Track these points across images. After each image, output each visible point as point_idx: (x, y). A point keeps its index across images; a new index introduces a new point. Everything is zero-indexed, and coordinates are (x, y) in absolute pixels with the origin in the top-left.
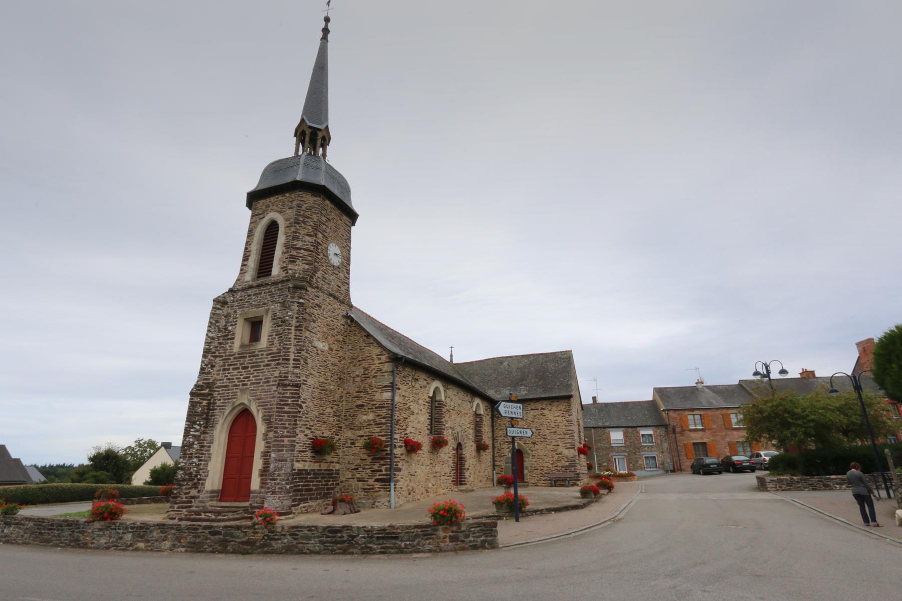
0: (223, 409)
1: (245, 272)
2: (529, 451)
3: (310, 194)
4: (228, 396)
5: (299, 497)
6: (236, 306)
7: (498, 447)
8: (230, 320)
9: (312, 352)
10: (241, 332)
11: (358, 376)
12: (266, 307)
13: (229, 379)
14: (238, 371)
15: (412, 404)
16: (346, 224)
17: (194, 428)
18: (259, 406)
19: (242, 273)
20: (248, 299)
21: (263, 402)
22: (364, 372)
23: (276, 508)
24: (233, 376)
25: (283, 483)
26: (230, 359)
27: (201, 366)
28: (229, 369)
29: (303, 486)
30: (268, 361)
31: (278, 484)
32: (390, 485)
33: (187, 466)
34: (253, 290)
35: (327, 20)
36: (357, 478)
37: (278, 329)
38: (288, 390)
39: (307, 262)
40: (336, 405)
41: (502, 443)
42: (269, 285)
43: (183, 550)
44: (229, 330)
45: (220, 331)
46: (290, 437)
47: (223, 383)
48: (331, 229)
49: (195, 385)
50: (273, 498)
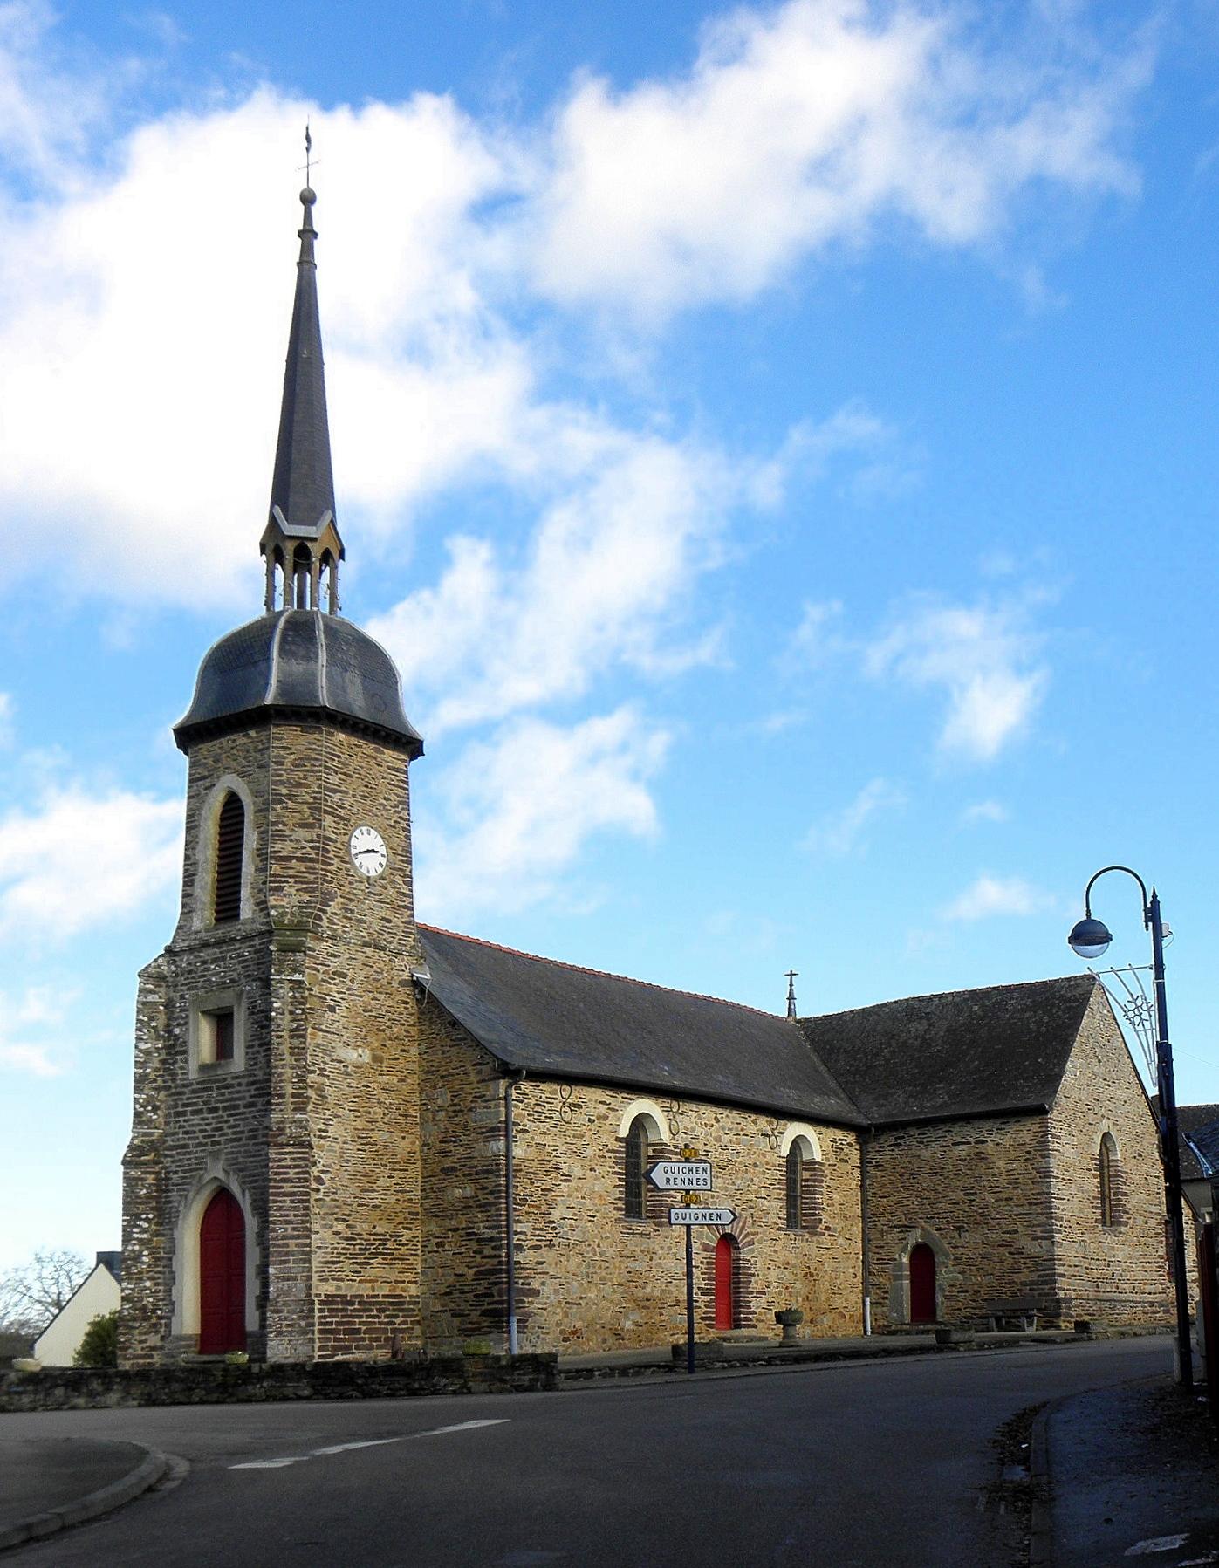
0: (184, 1190)
1: (190, 912)
2: (947, 1246)
3: (299, 729)
4: (189, 1165)
5: (332, 1343)
6: (182, 985)
7: (877, 1239)
8: (176, 1015)
9: (333, 1072)
10: (203, 1038)
11: (441, 1108)
12: (237, 989)
13: (186, 1133)
14: (202, 1116)
15: (564, 1158)
16: (393, 769)
17: (138, 1226)
18: (244, 1182)
19: (186, 913)
20: (204, 971)
21: (250, 1176)
22: (452, 1100)
23: (286, 1358)
24: (193, 1125)
25: (295, 1316)
26: (183, 1093)
27: (135, 1109)
28: (184, 1113)
29: (337, 1323)
30: (251, 1097)
31: (286, 1319)
32: (508, 1322)
33: (136, 1295)
34: (210, 951)
35: (308, 199)
36: (450, 1310)
37: (262, 1034)
38: (287, 1153)
39: (304, 886)
40: (401, 1170)
41: (885, 1228)
42: (236, 940)
43: (135, 1403)
44: (176, 1035)
45: (158, 1037)
46: (298, 1237)
47: (178, 1140)
48: (354, 796)
49: (129, 1146)
50: (278, 1342)
